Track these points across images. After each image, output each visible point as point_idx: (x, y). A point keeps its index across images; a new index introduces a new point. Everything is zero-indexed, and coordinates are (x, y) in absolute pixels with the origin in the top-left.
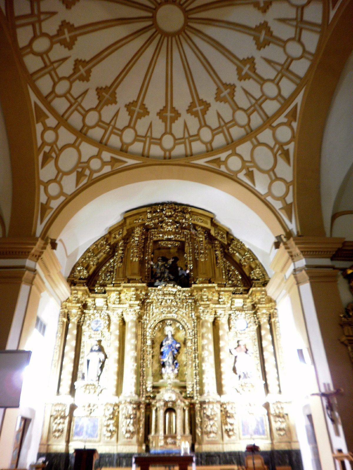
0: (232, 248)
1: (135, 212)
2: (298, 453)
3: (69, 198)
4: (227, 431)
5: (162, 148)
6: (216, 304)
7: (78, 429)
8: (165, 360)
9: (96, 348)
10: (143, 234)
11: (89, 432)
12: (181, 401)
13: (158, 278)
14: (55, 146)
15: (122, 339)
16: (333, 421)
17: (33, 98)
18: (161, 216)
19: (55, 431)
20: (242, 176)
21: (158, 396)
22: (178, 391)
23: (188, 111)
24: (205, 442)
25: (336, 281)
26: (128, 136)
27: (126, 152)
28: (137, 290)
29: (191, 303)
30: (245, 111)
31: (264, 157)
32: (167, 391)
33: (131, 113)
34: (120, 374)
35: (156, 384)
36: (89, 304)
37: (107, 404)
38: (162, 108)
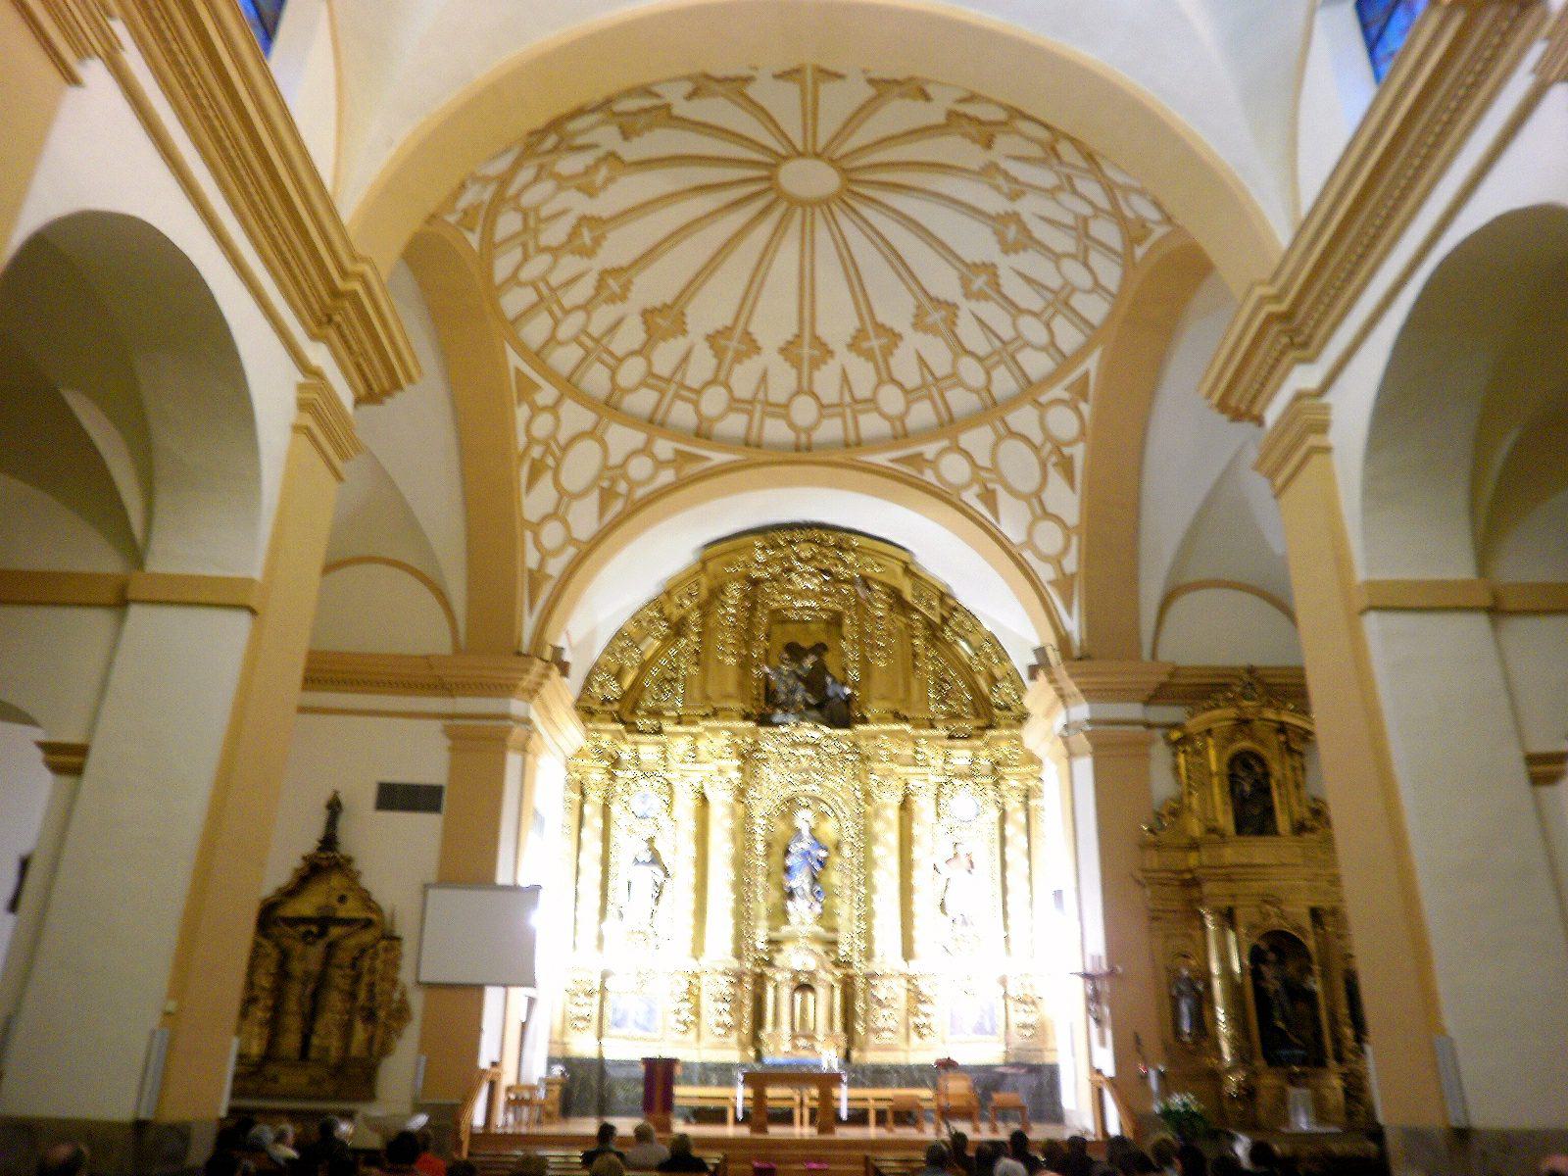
2: (1053, 1071)
3: (584, 548)
5: (791, 425)
8: (793, 884)
9: (647, 857)
10: (746, 597)
14: (552, 443)
16: (1098, 1021)
17: (514, 360)
18: (787, 558)
22: (819, 949)
26: (713, 402)
30: (980, 359)
31: (1020, 465)
32: (798, 950)
35: (775, 935)
36: (624, 757)
38: (790, 337)
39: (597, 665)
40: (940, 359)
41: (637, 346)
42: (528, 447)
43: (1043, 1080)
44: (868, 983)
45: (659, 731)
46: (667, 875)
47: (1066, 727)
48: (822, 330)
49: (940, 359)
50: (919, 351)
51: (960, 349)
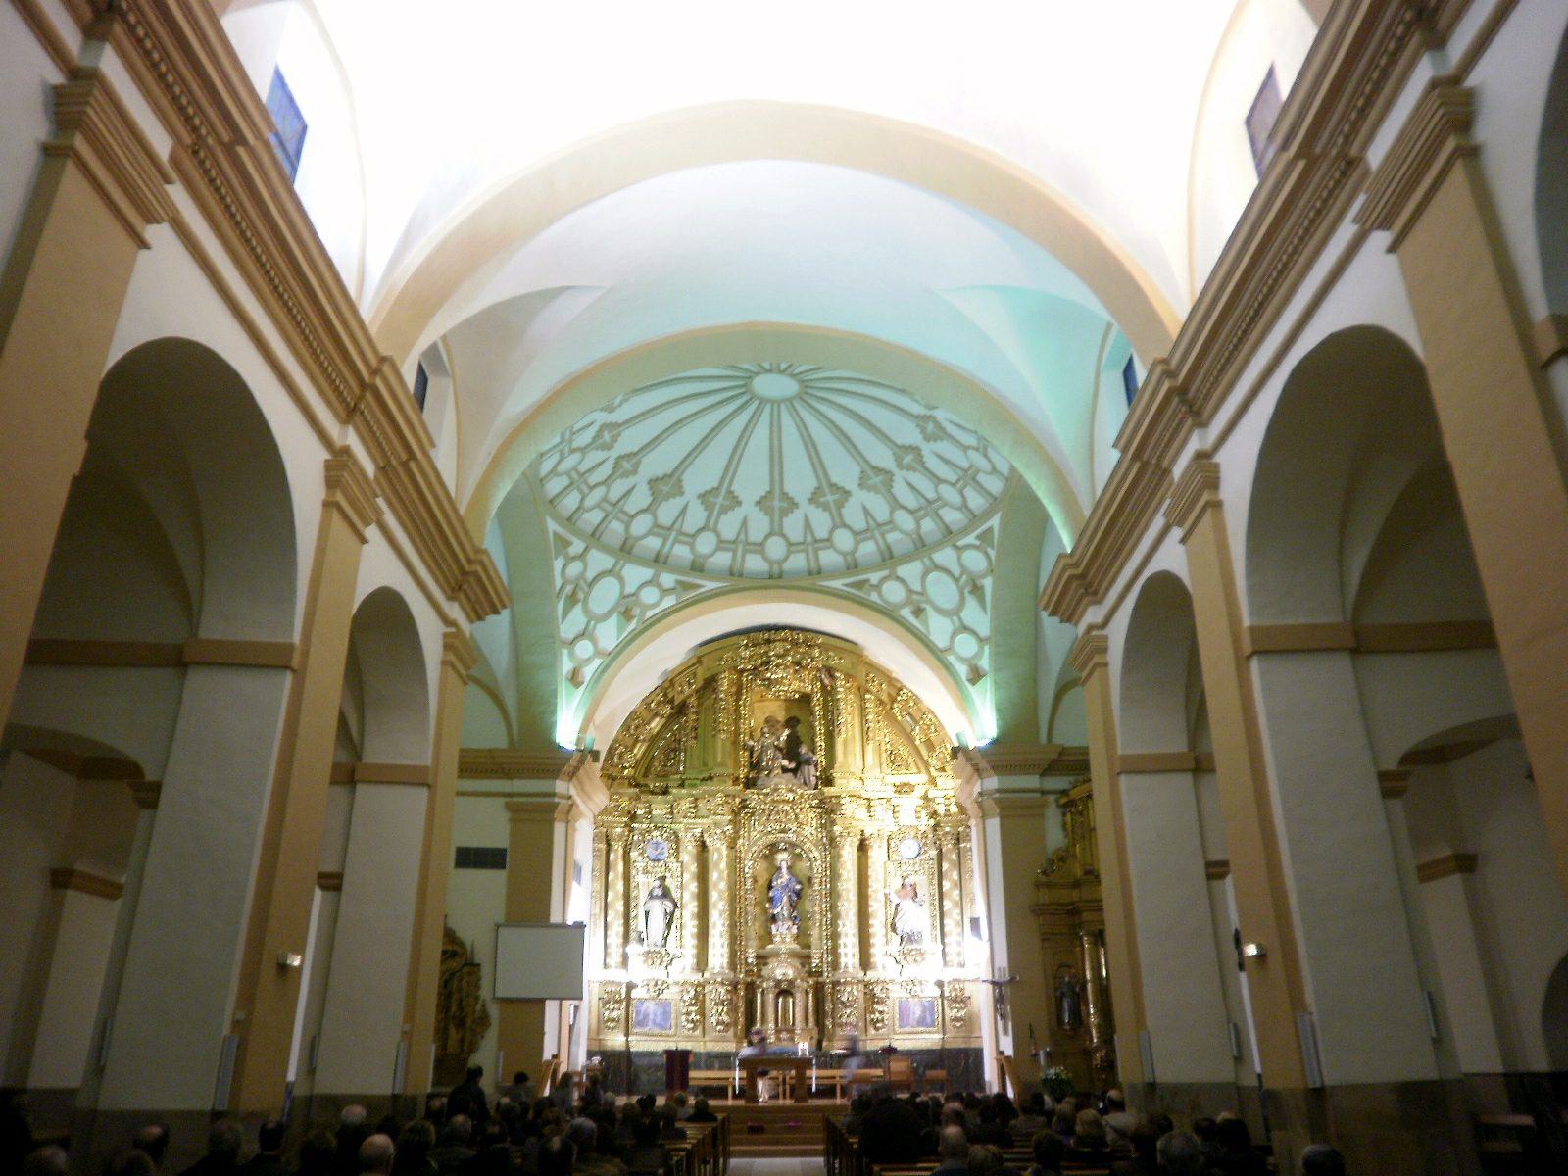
4: (874, 1023)
5: (766, 559)
7: (641, 1017)
11: (657, 1021)
12: (802, 980)
15: (703, 877)
16: (1003, 1017)
17: (552, 526)
19: (608, 1021)
20: (906, 613)
21: (765, 972)
22: (797, 963)
23: (811, 500)
25: (1042, 816)
26: (705, 544)
30: (912, 512)
31: (943, 591)
34: (703, 935)
39: (616, 741)
40: (880, 509)
41: (645, 506)
42: (563, 586)
43: (971, 1059)
44: (833, 988)
45: (665, 792)
46: (676, 906)
47: (981, 794)
48: (789, 488)
49: (880, 509)
50: (863, 504)
51: (896, 504)
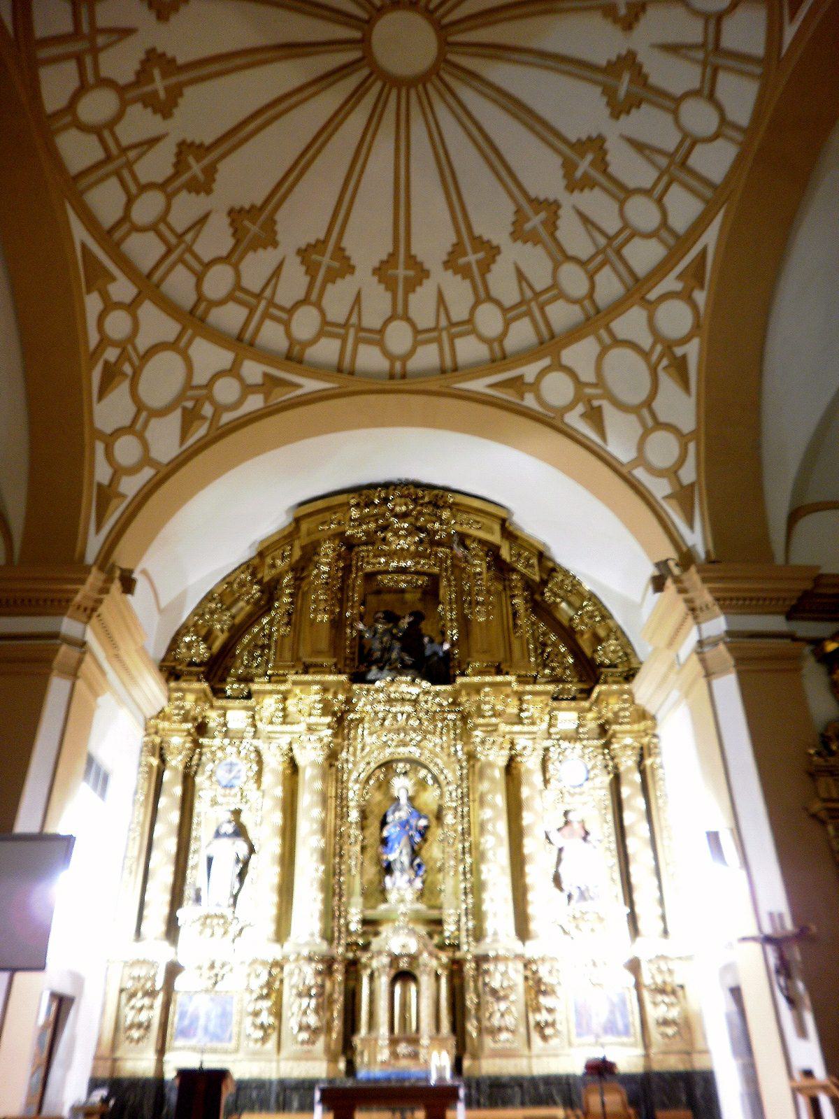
0: (551, 590)
1: (320, 504)
2: (708, 1079)
3: (164, 471)
4: (540, 1027)
5: (386, 353)
6: (513, 724)
7: (186, 1022)
8: (391, 857)
9: (229, 828)
10: (339, 557)
11: (211, 1028)
12: (431, 954)
13: (376, 662)
14: (130, 348)
15: (290, 807)
16: (792, 1002)
17: (79, 233)
18: (383, 515)
19: (131, 1027)
20: (574, 419)
21: (376, 943)
22: (422, 930)
23: (448, 264)
24: (486, 1051)
25: (798, 670)
26: (305, 324)
27: (300, 361)
28: (325, 690)
29: (454, 721)
30: (582, 264)
31: (627, 374)
32: (396, 930)
33: (311, 269)
34: (286, 890)
35: (371, 914)
36: (212, 724)
37: (254, 962)
38: (385, 257)
